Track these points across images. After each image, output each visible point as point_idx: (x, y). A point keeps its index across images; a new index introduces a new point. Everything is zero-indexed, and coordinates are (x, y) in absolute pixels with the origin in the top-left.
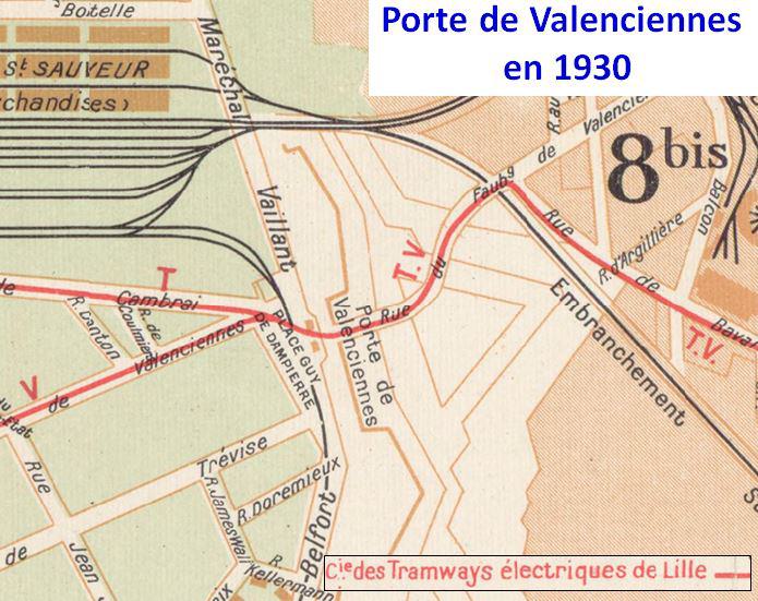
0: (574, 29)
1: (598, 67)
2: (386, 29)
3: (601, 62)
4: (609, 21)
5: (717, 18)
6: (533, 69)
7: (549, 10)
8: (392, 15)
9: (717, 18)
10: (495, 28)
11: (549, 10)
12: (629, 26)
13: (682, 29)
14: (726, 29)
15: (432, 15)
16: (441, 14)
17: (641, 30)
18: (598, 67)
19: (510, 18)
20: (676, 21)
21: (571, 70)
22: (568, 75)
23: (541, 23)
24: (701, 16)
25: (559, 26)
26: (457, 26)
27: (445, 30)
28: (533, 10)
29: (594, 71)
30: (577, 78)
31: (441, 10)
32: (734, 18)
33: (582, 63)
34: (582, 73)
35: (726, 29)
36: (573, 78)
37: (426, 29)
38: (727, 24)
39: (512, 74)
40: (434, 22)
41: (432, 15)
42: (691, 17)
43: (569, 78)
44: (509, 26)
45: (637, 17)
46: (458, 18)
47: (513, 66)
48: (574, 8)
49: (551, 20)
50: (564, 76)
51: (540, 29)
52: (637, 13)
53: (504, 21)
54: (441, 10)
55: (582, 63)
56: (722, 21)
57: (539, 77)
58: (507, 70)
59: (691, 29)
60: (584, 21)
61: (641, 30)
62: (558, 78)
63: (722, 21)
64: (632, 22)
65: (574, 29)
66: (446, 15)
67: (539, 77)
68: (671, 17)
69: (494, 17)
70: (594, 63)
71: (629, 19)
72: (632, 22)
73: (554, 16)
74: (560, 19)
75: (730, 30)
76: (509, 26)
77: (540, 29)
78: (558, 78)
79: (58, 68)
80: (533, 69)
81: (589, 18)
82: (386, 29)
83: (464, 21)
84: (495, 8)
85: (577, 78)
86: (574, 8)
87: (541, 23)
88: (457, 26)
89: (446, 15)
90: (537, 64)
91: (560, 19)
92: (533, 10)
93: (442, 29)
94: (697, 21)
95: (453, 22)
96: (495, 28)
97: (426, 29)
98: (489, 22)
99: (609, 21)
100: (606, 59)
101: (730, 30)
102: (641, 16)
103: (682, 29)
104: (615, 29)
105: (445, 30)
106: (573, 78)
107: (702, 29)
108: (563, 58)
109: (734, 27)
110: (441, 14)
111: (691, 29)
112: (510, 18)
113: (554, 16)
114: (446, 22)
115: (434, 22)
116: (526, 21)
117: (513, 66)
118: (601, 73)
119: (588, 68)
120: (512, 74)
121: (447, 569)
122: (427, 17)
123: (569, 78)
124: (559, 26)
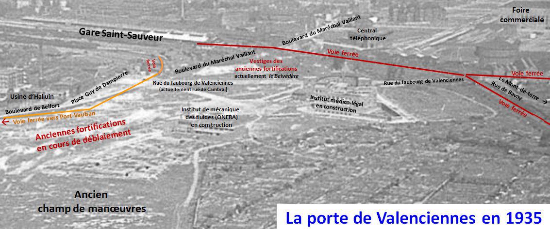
0: (397, 223)
1: (527, 218)
2: (309, 226)
3: (528, 215)
4: (414, 219)
5: (464, 218)
6: (496, 219)
7: (386, 213)
8: (312, 219)
9: (464, 218)
10: (360, 222)
11: (386, 213)
12: (423, 221)
13: (448, 223)
14: (468, 223)
15: (331, 216)
16: (336, 216)
17: (429, 223)
18: (527, 218)
19: (367, 218)
20: (445, 219)
21: (514, 219)
22: (512, 221)
23: (382, 220)
24: (456, 216)
25: (390, 221)
26: (344, 221)
27: (338, 223)
28: (378, 213)
29: (525, 220)
30: (517, 223)
31: (336, 214)
32: (472, 217)
33: (519, 216)
34: (519, 221)
35: (468, 223)
36: (515, 223)
37: (329, 222)
38: (469, 220)
39: (486, 221)
40: (332, 219)
41: (331, 216)
42: (452, 217)
43: (513, 223)
44: (367, 221)
45: (427, 217)
46: (344, 218)
47: (486, 218)
48: (397, 213)
49: (386, 218)
50: (510, 222)
51: (382, 222)
52: (427, 215)
53: (365, 219)
54: (336, 214)
55: (519, 216)
56: (467, 219)
57: (499, 222)
58: (484, 219)
59: (452, 223)
60: (402, 219)
61: (429, 223)
62: (508, 223)
63: (467, 219)
64: (424, 219)
65: (397, 223)
66: (338, 216)
67: (499, 222)
68: (442, 217)
69: (360, 217)
70: (525, 216)
71: (423, 218)
72: (424, 219)
73: (388, 216)
74: (391, 218)
75: (470, 223)
76: (367, 221)
77: (382, 222)
78: (508, 223)
79: (78, 195)
80: (496, 219)
81: (404, 218)
82: (309, 226)
83: (347, 219)
84: (361, 213)
85: (517, 223)
86: (397, 213)
87: (382, 220)
88: (344, 221)
89: (338, 216)
90: (498, 216)
91: (391, 218)
92: (378, 213)
93: (336, 222)
94: (455, 219)
95: (341, 219)
96: (360, 222)
97: (329, 222)
98: (358, 219)
99: (414, 219)
100: (530, 214)
101: (470, 223)
102: (429, 216)
103: (448, 223)
104: (416, 223)
105: (338, 223)
106: (515, 223)
107: (457, 223)
108: (510, 214)
109: (472, 221)
110: (336, 216)
111: (452, 223)
112: (367, 218)
113: (388, 216)
114: (338, 219)
115: (332, 219)
116: (375, 218)
117: (486, 218)
118: (528, 220)
119: (522, 218)
120: (486, 221)
121: (128, 211)
122: (329, 217)
123: (513, 223)
124: (390, 221)
